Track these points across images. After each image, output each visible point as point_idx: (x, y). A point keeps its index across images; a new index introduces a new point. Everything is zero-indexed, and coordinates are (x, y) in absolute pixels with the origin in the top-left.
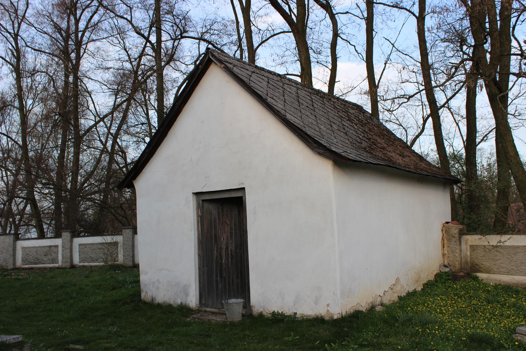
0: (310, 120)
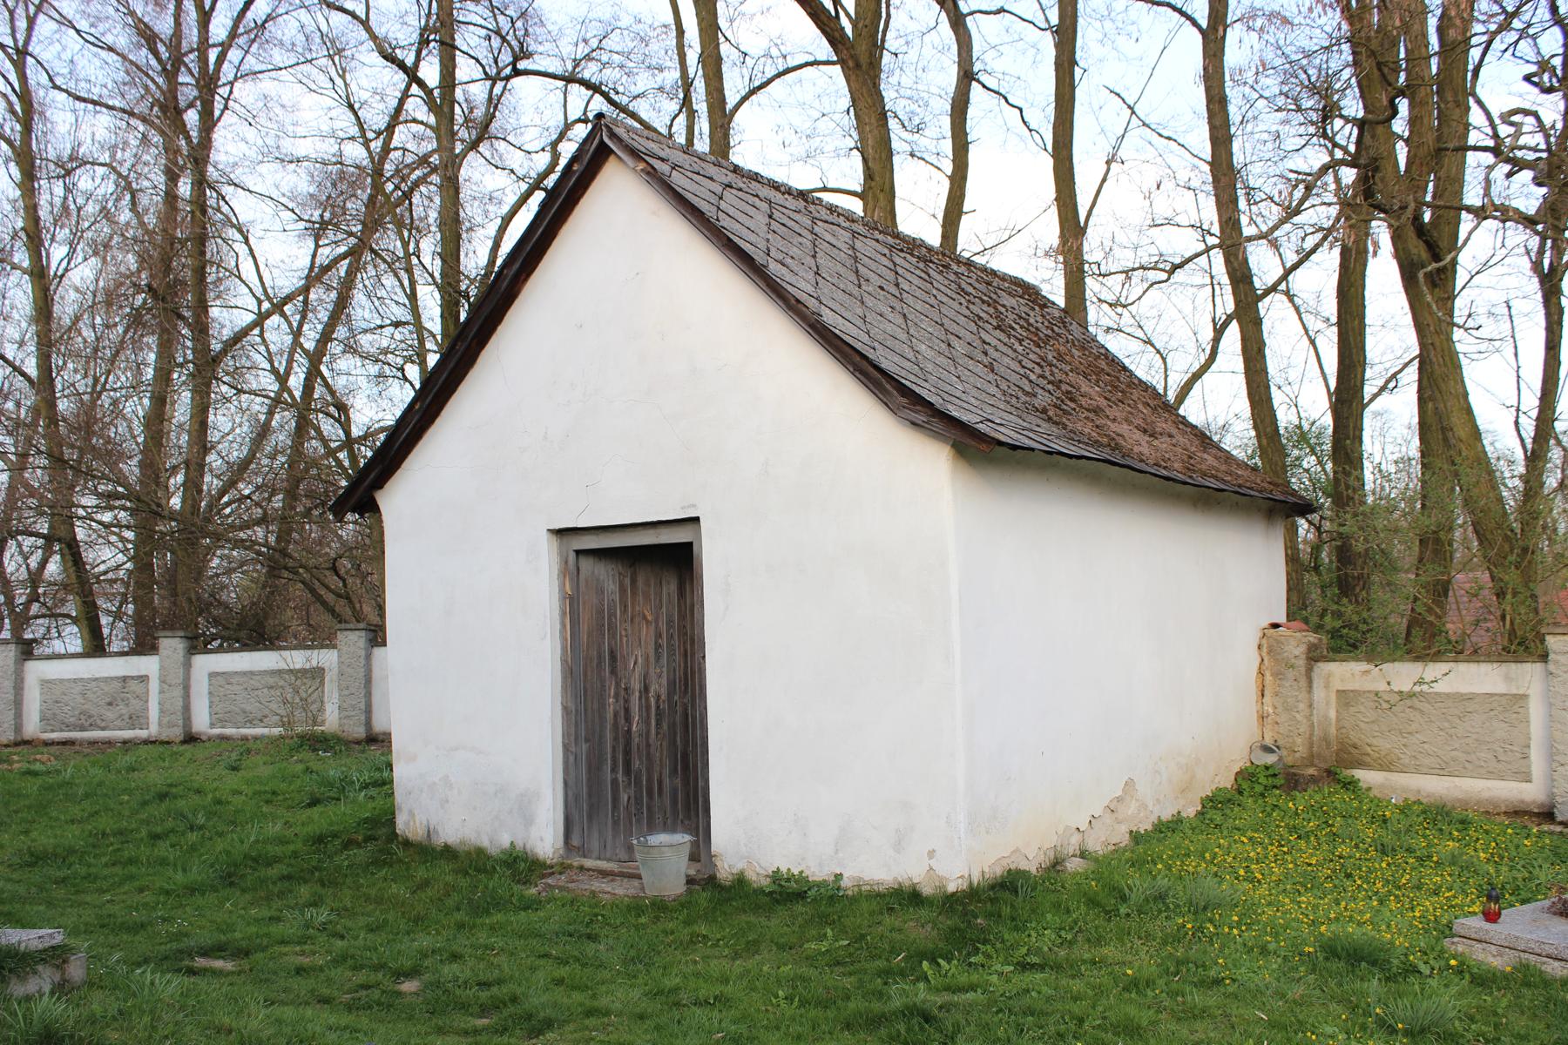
0: (889, 328)
